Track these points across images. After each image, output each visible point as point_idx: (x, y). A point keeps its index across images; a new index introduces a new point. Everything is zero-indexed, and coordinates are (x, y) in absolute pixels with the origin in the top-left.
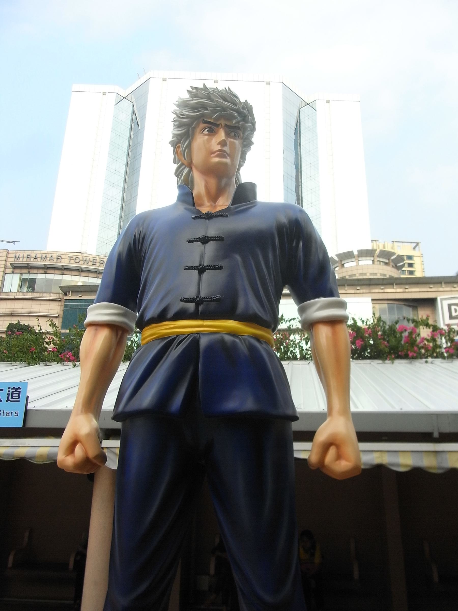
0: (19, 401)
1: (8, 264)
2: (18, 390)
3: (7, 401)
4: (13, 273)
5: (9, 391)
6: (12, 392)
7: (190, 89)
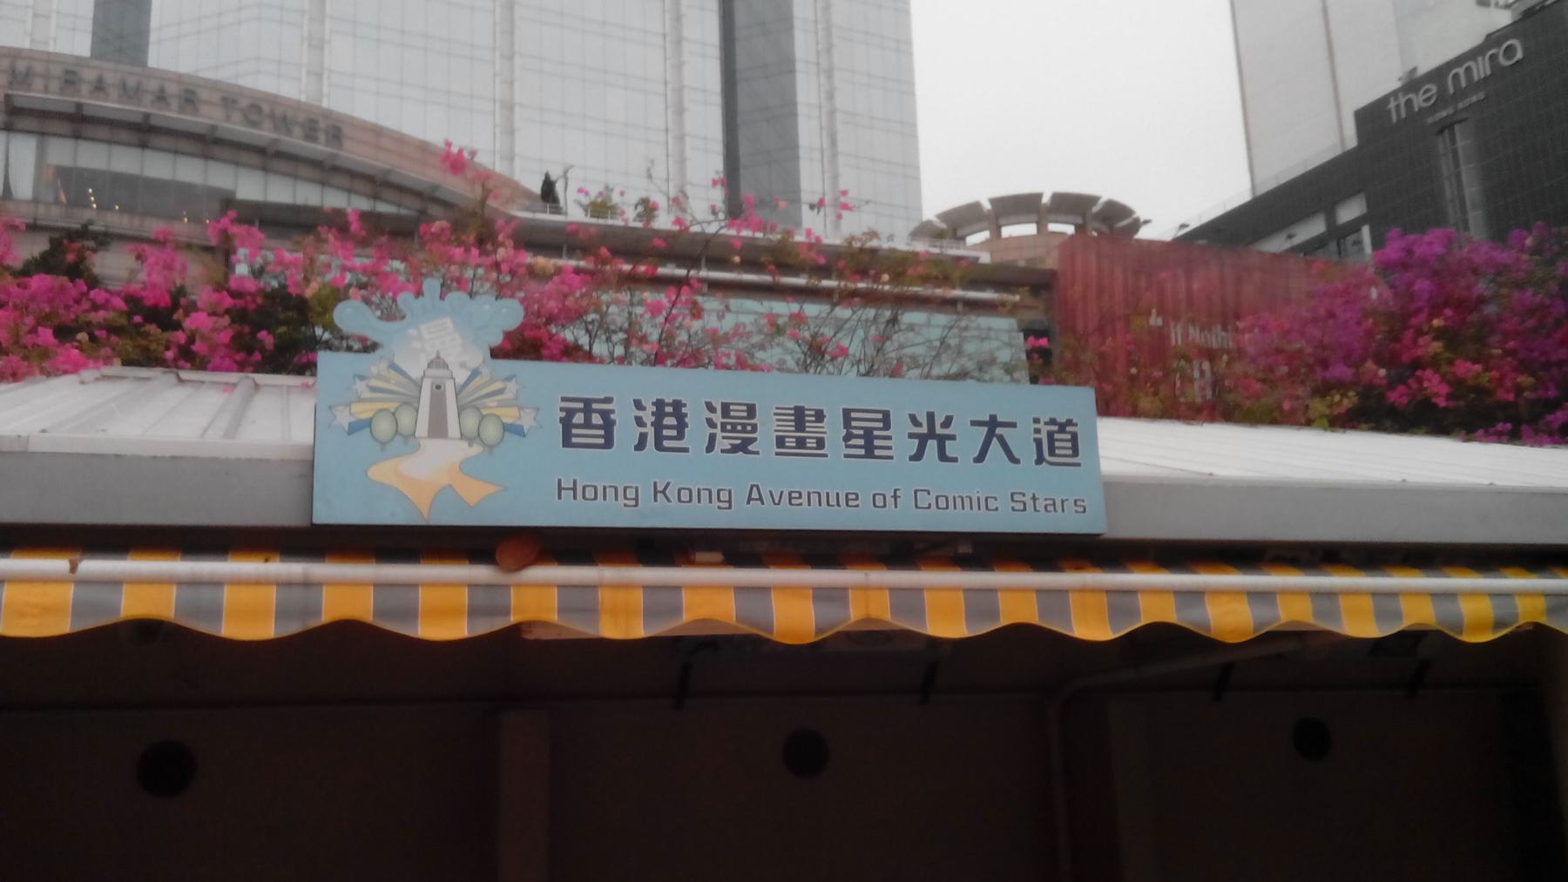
0: (891, 458)
2: (1069, 429)
6: (1050, 435)
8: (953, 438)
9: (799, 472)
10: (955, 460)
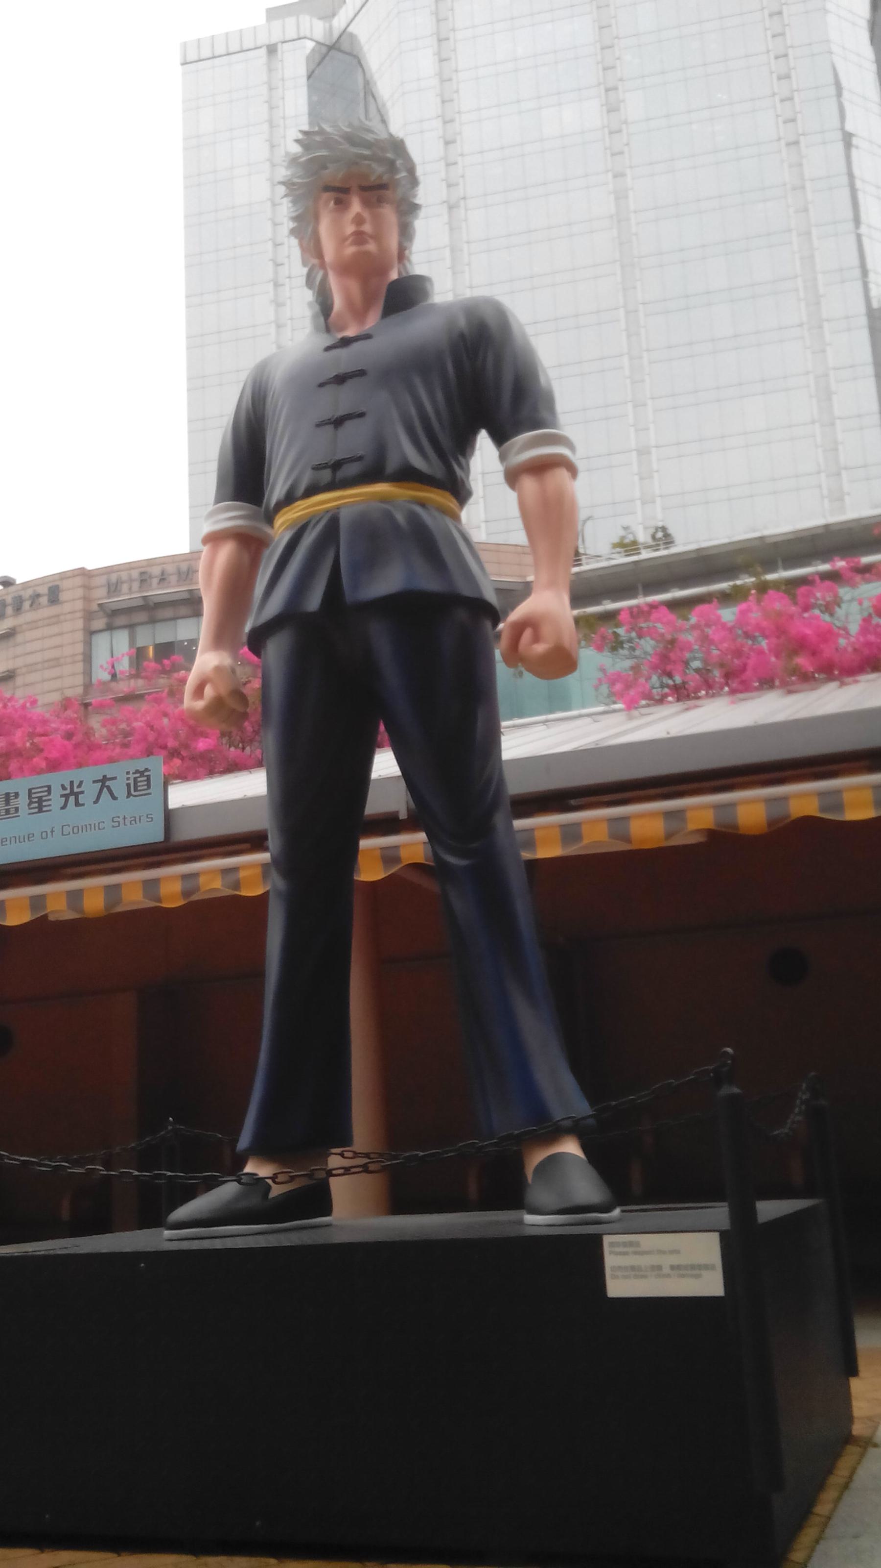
1: (95, 607)
3: (128, 797)
4: (110, 628)
5: (128, 779)
6: (135, 779)
7: (300, 136)
8: (82, 792)
9: (42, 821)
10: (83, 805)
